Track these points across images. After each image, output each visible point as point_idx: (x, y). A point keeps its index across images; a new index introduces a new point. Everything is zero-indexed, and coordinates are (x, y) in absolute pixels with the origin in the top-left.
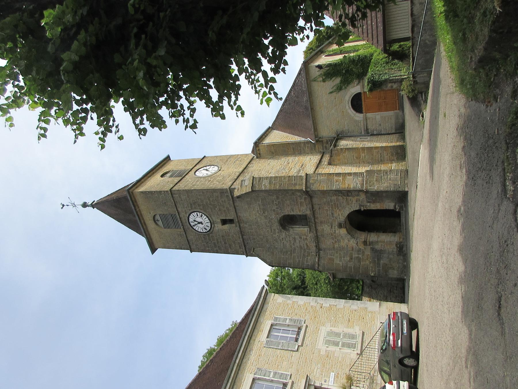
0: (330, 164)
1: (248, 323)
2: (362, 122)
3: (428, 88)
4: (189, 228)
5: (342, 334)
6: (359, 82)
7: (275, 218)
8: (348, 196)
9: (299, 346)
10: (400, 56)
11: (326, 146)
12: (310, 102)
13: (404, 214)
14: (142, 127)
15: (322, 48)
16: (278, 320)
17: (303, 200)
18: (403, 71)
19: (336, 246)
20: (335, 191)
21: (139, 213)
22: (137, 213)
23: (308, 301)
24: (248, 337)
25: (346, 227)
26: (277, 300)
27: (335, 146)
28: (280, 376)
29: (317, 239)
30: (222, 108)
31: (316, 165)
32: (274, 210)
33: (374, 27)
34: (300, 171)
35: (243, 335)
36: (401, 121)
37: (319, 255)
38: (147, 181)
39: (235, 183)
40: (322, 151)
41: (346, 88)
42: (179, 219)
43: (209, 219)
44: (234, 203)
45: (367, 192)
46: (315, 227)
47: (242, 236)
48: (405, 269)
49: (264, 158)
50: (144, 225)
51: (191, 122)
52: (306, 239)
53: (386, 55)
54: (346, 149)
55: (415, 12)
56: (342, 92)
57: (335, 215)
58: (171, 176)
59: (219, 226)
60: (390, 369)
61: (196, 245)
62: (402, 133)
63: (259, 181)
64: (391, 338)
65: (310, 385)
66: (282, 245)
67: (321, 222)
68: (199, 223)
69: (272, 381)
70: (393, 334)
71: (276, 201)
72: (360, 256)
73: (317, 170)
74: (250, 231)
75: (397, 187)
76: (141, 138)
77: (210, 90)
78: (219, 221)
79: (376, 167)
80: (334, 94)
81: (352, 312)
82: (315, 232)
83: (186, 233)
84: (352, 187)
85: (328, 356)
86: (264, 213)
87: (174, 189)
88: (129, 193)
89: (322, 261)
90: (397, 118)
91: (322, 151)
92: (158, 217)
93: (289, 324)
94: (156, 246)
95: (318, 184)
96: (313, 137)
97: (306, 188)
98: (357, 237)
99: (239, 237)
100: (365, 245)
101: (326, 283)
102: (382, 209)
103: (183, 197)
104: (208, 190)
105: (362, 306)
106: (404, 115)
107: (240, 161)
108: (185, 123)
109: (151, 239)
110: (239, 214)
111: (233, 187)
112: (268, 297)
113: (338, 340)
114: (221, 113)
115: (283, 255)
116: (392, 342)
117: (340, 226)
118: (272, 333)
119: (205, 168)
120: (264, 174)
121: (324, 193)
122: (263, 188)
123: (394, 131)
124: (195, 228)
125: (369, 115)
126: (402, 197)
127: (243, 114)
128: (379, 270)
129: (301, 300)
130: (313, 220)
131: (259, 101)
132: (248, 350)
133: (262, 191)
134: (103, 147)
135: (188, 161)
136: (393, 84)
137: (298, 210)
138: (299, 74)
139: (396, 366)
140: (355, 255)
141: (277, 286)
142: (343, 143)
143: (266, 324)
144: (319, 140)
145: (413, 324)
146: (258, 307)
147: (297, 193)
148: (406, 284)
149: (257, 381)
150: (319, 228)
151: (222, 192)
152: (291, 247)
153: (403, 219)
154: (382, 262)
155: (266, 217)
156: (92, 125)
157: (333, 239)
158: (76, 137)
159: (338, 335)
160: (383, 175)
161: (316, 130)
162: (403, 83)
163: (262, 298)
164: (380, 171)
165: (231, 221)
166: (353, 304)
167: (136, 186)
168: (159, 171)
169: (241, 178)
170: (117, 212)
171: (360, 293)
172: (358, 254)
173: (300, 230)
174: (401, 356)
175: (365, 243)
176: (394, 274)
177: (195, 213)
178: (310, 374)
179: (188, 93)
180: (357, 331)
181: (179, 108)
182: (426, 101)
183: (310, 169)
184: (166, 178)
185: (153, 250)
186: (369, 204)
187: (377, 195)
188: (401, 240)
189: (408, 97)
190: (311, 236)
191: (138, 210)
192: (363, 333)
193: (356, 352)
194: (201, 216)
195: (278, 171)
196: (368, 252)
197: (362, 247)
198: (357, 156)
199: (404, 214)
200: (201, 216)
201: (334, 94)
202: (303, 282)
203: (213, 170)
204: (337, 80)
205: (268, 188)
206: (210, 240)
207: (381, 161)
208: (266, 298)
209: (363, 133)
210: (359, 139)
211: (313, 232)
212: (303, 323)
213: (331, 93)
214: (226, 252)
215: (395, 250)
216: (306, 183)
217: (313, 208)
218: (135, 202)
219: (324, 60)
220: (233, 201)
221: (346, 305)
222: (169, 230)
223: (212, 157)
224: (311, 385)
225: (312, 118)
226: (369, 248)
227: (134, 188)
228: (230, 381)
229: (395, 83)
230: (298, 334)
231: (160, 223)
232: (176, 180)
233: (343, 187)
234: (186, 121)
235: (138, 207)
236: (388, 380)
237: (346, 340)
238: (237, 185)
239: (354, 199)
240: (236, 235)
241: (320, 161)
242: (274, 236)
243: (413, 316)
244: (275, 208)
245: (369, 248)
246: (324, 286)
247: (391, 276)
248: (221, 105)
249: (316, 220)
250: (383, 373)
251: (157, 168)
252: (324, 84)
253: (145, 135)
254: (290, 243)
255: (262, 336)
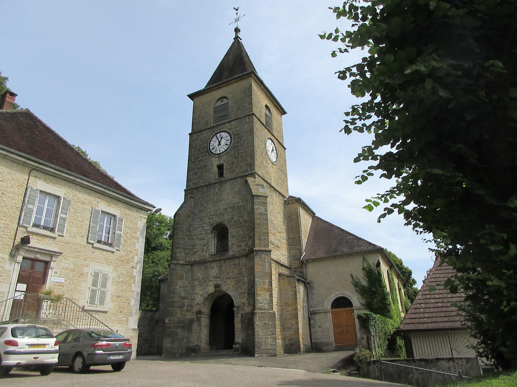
0: (280, 275)
1: (118, 191)
2: (323, 308)
3: (364, 377)
4: (214, 132)
5: (105, 289)
6: (363, 305)
7: (225, 219)
8: (249, 294)
9: (93, 244)
10: (392, 347)
11: (298, 271)
12: (342, 255)
13: (230, 353)
14: (348, 74)
15: (394, 268)
16: (120, 222)
17: (243, 247)
18: (378, 351)
19: (196, 283)
20: (254, 281)
21: (230, 82)
22: (231, 80)
23: (139, 254)
24: (103, 191)
25: (215, 292)
26: (141, 221)
27: (299, 280)
28: (62, 225)
29: (203, 262)
30: (366, 159)
31: (278, 261)
32: (232, 218)
33: (422, 320)
34: (273, 244)
35: (105, 186)
36: (325, 348)
37: (186, 264)
38: (261, 91)
39: (260, 178)
40: (293, 267)
41: (357, 291)
42: (223, 122)
43: (223, 152)
44: (240, 177)
45: (253, 313)
46: (215, 261)
47: (206, 186)
48: (173, 356)
49: (284, 208)
50: (218, 87)
51: (351, 127)
52: (203, 251)
53: (392, 333)
54: (296, 291)
55: (440, 363)
56: (353, 288)
57: (228, 281)
58: (266, 115)
59: (216, 162)
60: (70, 342)
61: (197, 139)
62: (312, 350)
63: (263, 203)
64: (104, 343)
65: (52, 256)
66: (196, 226)
67: (220, 267)
68: (219, 142)
69: (56, 216)
70: (109, 345)
71: (242, 220)
72: (185, 308)
73: (274, 262)
74: (212, 193)
75: (259, 346)
76: (336, 73)
77: (390, 145)
78: (222, 162)
79: (278, 322)
80: (351, 279)
81: (128, 300)
82: (210, 260)
83: (209, 129)
84: (259, 298)
85: (81, 275)
86: (230, 207)
87: (254, 117)
88: (251, 73)
89: (180, 268)
90: (328, 344)
91: (293, 267)
92: (225, 101)
93: (116, 234)
94: (196, 99)
95: (260, 263)
96: (306, 258)
97: (256, 250)
98: (205, 304)
99: (204, 183)
100: (197, 312)
101: (154, 273)
102: (235, 330)
103: (246, 126)
104: (253, 151)
105: (134, 311)
106: (331, 351)
107: (281, 184)
108: (351, 121)
109: (203, 94)
110: (228, 183)
111: (256, 176)
112: (143, 211)
113: (99, 286)
114: (361, 158)
115: (186, 228)
116: (100, 343)
117: (217, 286)
118: (106, 216)
119: (274, 149)
120: (270, 207)
121: (252, 269)
122: (256, 207)
123: (313, 341)
124: (214, 138)
125: (330, 315)
126: (248, 351)
127: (359, 182)
128: (171, 328)
129: (140, 246)
130: (222, 258)
131: (369, 198)
132: (89, 191)
133: (253, 205)
134: (322, 37)
135: (281, 132)
136: (366, 340)
137: (233, 242)
138: (370, 244)
139: (74, 349)
140: (186, 302)
141: (154, 221)
142: (301, 289)
143: (115, 210)
144: (303, 264)
145: (118, 366)
146: (133, 202)
147: (251, 242)
148: (156, 357)
149: (56, 201)
150: (214, 264)
151: (252, 165)
152: (195, 235)
153: (224, 352)
154: (180, 330)
155: (226, 209)
156: (347, 25)
157: (203, 278)
158: (336, 10)
159: (104, 285)
160: (271, 331)
161: (314, 260)
162: (368, 351)
163: (143, 206)
164: (275, 328)
165: (221, 174)
166: (136, 300)
167: (257, 80)
168: (271, 103)
169: (265, 184)
170: (230, 61)
171: (143, 308)
172: (187, 306)
173: (212, 245)
174: (85, 354)
175: (199, 312)
176: (167, 344)
177: (230, 139)
178: (63, 256)
179: (379, 125)
180: (109, 305)
181: (368, 114)
182: (350, 374)
183: (275, 255)
184: (264, 111)
185: (192, 96)
186: (240, 316)
187: (249, 323)
188: (203, 351)
189: (353, 356)
190: (205, 255)
191: (233, 81)
192: (105, 312)
193: (86, 305)
194: (226, 144)
195: (272, 223)
196: (189, 316)
197: (195, 309)
198: (288, 303)
199: (230, 353)
200: (226, 144)
201: (351, 279)
202: (155, 249)
203: (273, 157)
204: (364, 283)
205: (256, 211)
206: (202, 153)
207: (283, 328)
208: (142, 209)
209: (311, 309)
210: (305, 304)
211: (211, 258)
212: (117, 248)
213: (352, 276)
214: (189, 169)
215: (192, 344)
216: (262, 251)
217: (235, 258)
218: (241, 78)
219: (384, 269)
220: (242, 176)
221: (135, 294)
222: (212, 112)
223: (285, 156)
224: (52, 257)
225: (326, 257)
226: (194, 316)
227: (256, 78)
228: (57, 172)
229: (368, 342)
230: (106, 243)
231: (219, 103)
232: (263, 120)
233: (258, 289)
234: (353, 122)
235: (235, 82)
236: (59, 340)
237: (98, 294)
238: (258, 180)
239: (245, 300)
240: (207, 179)
241: (282, 265)
242: (206, 218)
243: (127, 366)
244: (235, 218)
245: (194, 316)
246: (151, 270)
247: (165, 340)
248: (370, 158)
249: (222, 261)
250: (66, 334)
251: (274, 102)
252: (361, 269)
253: (339, 77)
254: (199, 235)
255: (103, 205)
